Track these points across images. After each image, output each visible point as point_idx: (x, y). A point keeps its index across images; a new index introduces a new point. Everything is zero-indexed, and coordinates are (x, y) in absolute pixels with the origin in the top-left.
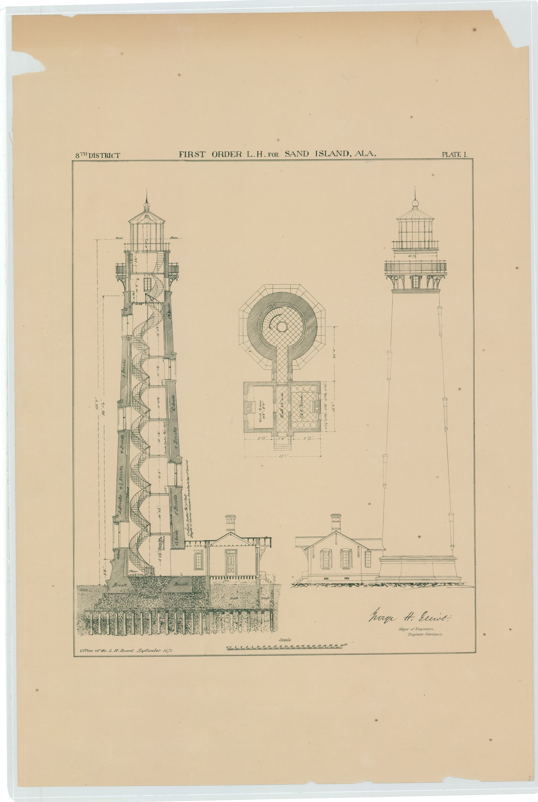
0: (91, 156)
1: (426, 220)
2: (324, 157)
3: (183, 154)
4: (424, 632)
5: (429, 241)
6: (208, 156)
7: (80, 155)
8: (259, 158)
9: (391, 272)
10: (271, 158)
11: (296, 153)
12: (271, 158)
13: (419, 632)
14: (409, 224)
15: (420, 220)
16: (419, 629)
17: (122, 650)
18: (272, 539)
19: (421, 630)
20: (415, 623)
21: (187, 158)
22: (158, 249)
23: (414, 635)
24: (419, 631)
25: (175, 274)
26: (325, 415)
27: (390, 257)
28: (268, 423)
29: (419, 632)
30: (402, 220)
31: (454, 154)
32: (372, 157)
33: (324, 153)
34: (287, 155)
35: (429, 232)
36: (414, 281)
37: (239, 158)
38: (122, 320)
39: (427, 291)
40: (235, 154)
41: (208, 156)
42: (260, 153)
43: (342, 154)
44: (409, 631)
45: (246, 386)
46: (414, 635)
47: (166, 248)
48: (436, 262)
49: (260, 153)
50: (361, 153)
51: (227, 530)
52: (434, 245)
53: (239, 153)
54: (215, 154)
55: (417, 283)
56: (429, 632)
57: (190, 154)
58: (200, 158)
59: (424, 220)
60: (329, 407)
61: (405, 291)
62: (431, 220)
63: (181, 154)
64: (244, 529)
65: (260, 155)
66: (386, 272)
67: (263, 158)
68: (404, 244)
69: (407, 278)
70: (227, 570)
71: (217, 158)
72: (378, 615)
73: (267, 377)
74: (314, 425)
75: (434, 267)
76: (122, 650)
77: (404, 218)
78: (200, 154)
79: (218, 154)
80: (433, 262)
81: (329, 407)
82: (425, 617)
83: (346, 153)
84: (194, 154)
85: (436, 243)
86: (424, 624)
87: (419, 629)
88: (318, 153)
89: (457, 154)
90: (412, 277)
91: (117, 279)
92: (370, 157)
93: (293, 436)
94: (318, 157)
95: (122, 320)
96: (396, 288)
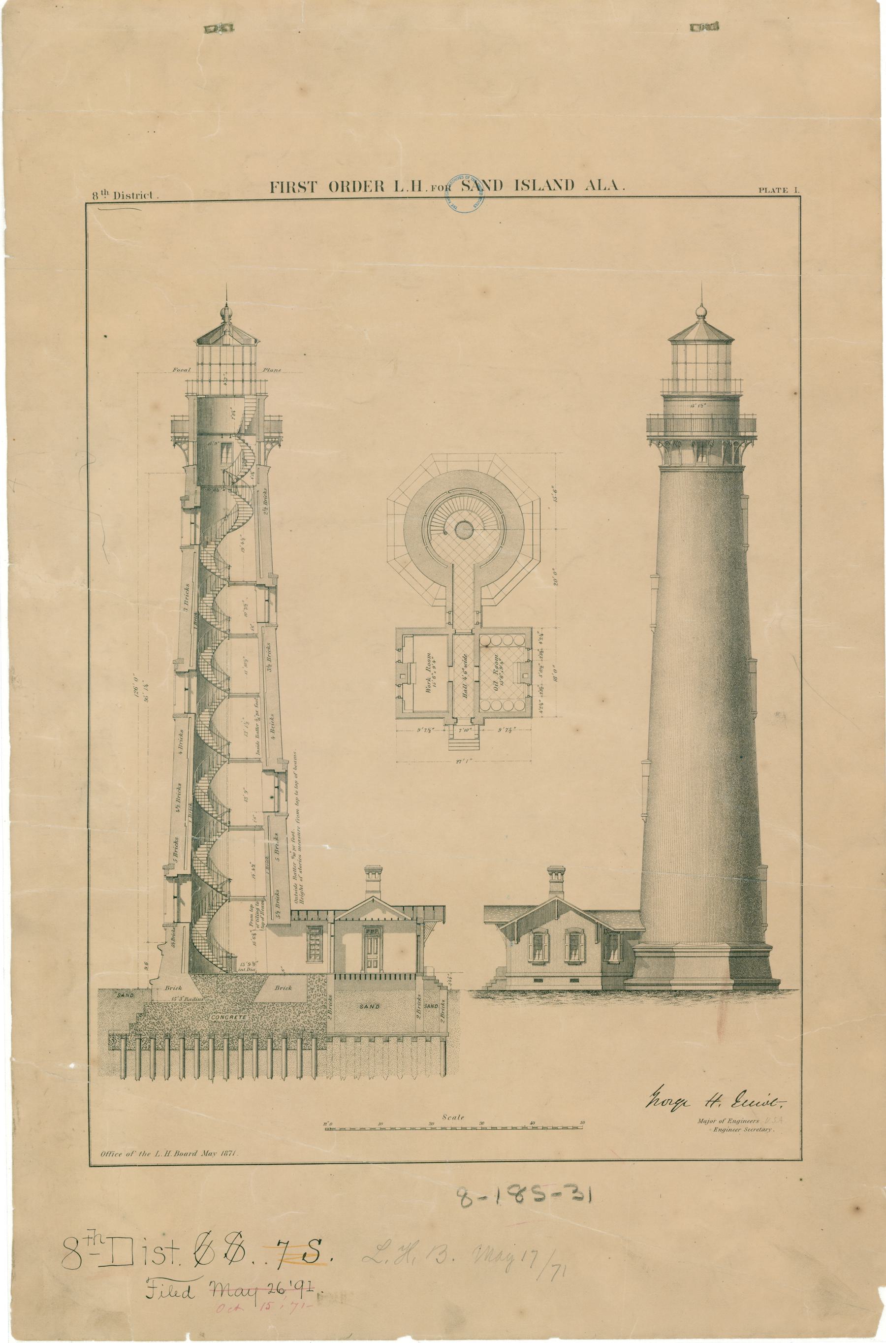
2: (531, 193)
4: (742, 1126)
6: (322, 190)
8: (416, 193)
11: (553, 185)
13: (733, 1126)
16: (734, 1121)
18: (447, 908)
19: (738, 1122)
20: (724, 1110)
22: (247, 391)
25: (277, 435)
26: (541, 689)
28: (437, 701)
29: (733, 1126)
33: (531, 185)
34: (466, 188)
35: (251, 364)
38: (182, 517)
42: (416, 183)
43: (492, 188)
44: (716, 1124)
45: (405, 635)
47: (259, 388)
49: (416, 183)
51: (367, 892)
53: (379, 183)
56: (750, 1126)
60: (548, 672)
64: (398, 890)
65: (416, 188)
66: (648, 434)
68: (682, 384)
70: (366, 964)
73: (438, 619)
74: (520, 706)
76: (177, 1153)
78: (308, 187)
79: (342, 186)
81: (548, 672)
82: (742, 1101)
84: (297, 187)
85: (263, 383)
86: (741, 1113)
87: (734, 1121)
88: (520, 185)
91: (172, 443)
92: (613, 192)
93: (484, 724)
94: (520, 193)
95: (182, 517)
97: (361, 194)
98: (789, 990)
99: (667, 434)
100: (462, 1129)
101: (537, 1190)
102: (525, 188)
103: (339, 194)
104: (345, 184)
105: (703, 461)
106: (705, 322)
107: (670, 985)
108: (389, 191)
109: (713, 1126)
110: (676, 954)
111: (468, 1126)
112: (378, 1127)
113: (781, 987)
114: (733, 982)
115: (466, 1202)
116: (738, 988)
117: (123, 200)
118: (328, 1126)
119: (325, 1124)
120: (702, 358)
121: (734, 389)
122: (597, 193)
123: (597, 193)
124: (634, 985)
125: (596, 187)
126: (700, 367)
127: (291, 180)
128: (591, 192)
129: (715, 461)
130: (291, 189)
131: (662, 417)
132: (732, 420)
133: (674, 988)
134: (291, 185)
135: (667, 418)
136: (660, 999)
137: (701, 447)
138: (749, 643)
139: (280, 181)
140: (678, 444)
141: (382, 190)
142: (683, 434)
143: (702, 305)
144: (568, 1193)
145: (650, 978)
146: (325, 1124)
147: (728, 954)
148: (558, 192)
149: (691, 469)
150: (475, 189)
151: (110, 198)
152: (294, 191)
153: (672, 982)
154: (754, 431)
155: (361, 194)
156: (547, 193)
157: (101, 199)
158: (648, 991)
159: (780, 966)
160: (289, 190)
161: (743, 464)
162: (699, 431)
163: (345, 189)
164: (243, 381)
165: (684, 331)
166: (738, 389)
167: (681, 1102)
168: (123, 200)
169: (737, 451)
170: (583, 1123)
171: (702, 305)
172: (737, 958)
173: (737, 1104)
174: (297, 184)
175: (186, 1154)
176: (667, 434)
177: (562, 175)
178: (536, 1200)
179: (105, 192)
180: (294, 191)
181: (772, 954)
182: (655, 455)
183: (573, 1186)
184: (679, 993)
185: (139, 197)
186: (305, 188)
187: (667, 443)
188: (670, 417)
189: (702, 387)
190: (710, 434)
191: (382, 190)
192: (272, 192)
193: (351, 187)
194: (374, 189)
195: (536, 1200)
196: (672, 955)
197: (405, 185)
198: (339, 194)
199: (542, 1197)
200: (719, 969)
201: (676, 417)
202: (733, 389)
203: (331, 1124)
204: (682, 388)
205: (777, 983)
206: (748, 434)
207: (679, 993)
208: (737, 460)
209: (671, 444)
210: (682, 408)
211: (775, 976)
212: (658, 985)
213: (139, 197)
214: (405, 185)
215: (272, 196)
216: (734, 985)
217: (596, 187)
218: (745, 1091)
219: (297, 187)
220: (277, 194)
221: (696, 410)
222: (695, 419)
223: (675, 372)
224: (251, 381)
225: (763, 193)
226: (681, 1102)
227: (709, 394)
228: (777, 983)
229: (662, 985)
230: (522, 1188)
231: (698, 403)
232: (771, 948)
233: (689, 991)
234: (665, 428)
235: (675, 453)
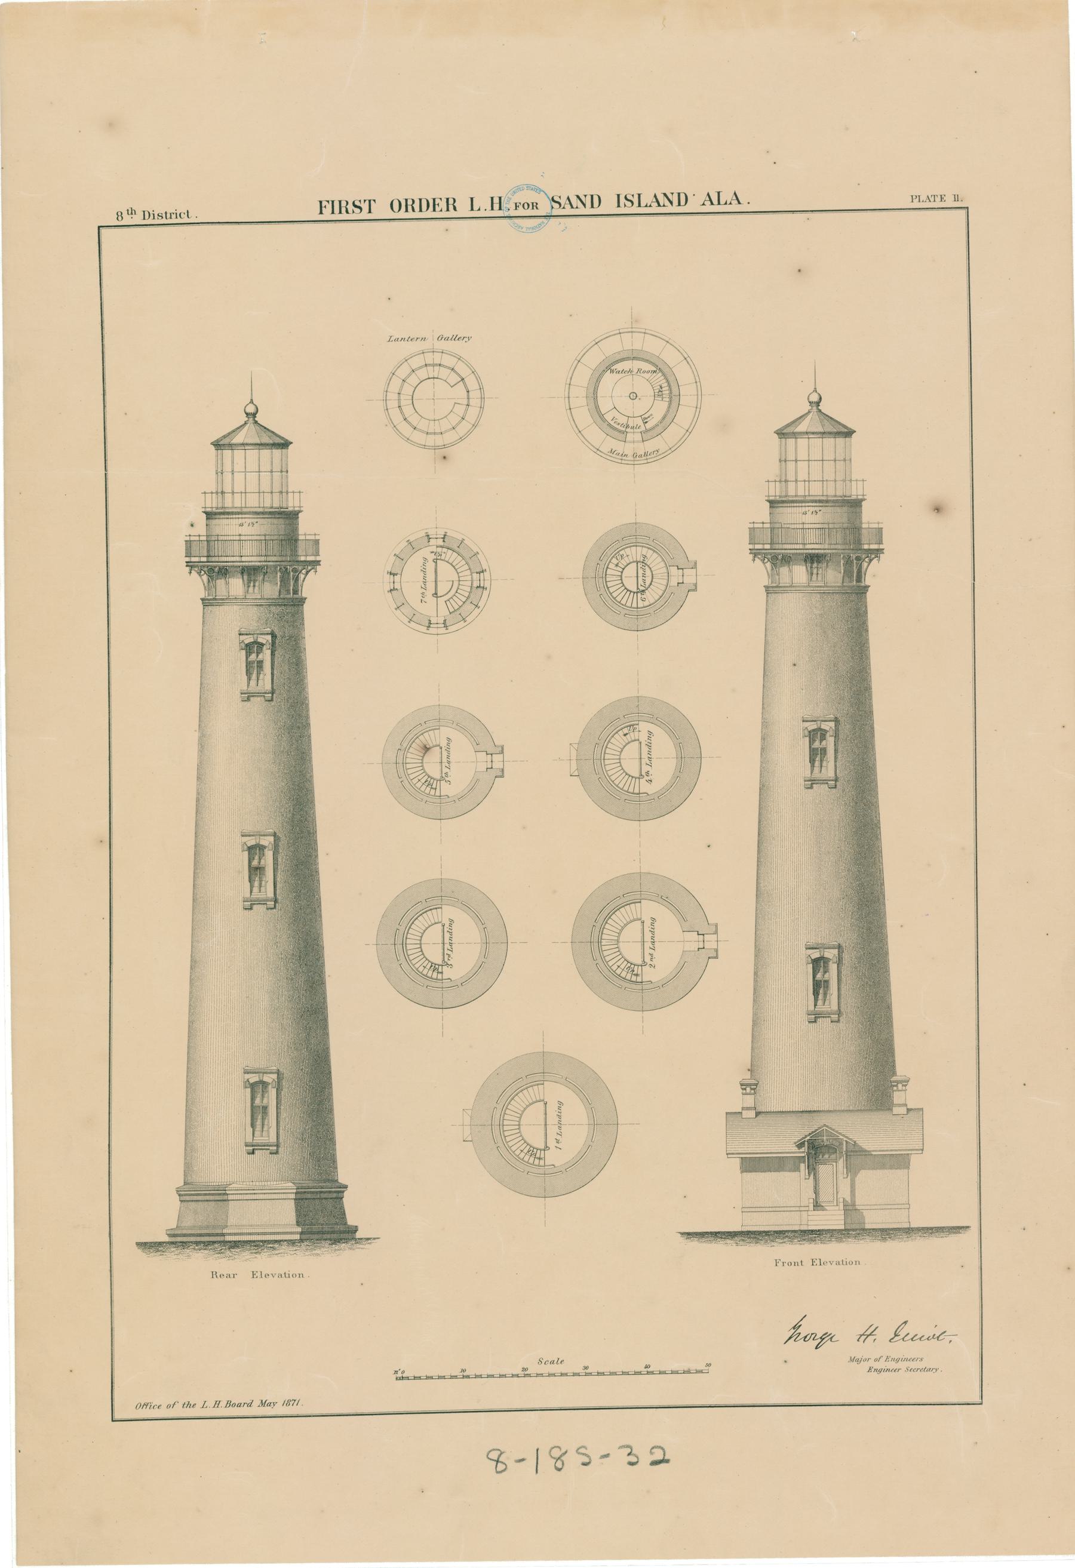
2: (635, 209)
4: (902, 1365)
6: (381, 210)
7: (125, 215)
8: (497, 213)
10: (521, 212)
11: (661, 198)
13: (891, 1365)
16: (893, 1359)
17: (229, 1404)
19: (897, 1361)
21: (337, 217)
23: (879, 1371)
24: (893, 1363)
32: (739, 208)
34: (556, 206)
37: (452, 213)
42: (496, 200)
43: (675, 202)
46: (879, 1371)
49: (496, 200)
50: (496, 203)
53: (451, 201)
56: (913, 1365)
58: (365, 215)
65: (496, 206)
68: (228, 497)
72: (803, 1331)
76: (229, 1404)
78: (365, 207)
79: (406, 205)
82: (902, 1334)
84: (350, 207)
86: (901, 1349)
87: (893, 1359)
92: (735, 207)
97: (430, 214)
98: (368, 1239)
99: (210, 559)
100: (562, 1375)
101: (582, 1450)
102: (629, 204)
103: (402, 214)
104: (410, 202)
105: (255, 593)
106: (256, 422)
107: (223, 1235)
108: (463, 209)
109: (865, 1366)
110: (230, 1197)
111: (570, 1371)
112: (521, 1373)
113: (358, 1235)
114: (299, 1230)
115: (501, 1467)
116: (304, 1237)
117: (154, 220)
118: (399, 1375)
119: (396, 1372)
120: (252, 466)
121: (292, 504)
122: (716, 208)
123: (716, 208)
124: (230, 1234)
125: (715, 201)
126: (250, 478)
127: (343, 198)
128: (708, 208)
129: (270, 589)
130: (343, 210)
131: (204, 538)
132: (291, 539)
133: (228, 1238)
134: (344, 204)
135: (210, 541)
136: (211, 1252)
137: (250, 572)
138: (314, 813)
139: (330, 199)
140: (224, 572)
141: (455, 209)
142: (225, 559)
143: (252, 402)
144: (623, 1456)
145: (201, 1228)
146: (396, 1372)
147: (293, 1196)
148: (582, 210)
149: (242, 601)
150: (568, 206)
151: (138, 219)
152: (347, 212)
153: (225, 1231)
155: (430, 214)
156: (655, 209)
157: (127, 220)
158: (197, 1243)
159: (355, 1210)
160: (339, 211)
161: (304, 595)
162: (250, 556)
163: (410, 208)
165: (229, 434)
166: (297, 504)
167: (827, 1337)
168: (154, 220)
169: (297, 579)
170: (709, 1365)
171: (252, 402)
172: (302, 1199)
173: (897, 1338)
174: (351, 204)
176: (210, 559)
177: (673, 187)
179: (132, 212)
180: (347, 212)
181: (347, 1195)
182: (196, 585)
183: (628, 1446)
184: (235, 1245)
185: (174, 216)
186: (360, 208)
187: (211, 570)
188: (213, 538)
189: (253, 502)
190: (263, 559)
191: (455, 209)
192: (321, 213)
193: (416, 206)
194: (445, 208)
195: (584, 1464)
196: (225, 1197)
197: (482, 202)
198: (402, 214)
199: (587, 1460)
200: (282, 1215)
201: (221, 538)
202: (290, 504)
203: (403, 1372)
204: (228, 503)
205: (355, 1230)
206: (309, 558)
207: (235, 1245)
208: (295, 592)
209: (215, 572)
210: (228, 527)
211: (351, 1221)
212: (209, 1235)
213: (174, 216)
214: (482, 202)
215: (321, 217)
216: (302, 1233)
217: (715, 201)
218: (905, 1322)
219: (350, 207)
220: (327, 214)
221: (246, 530)
222: (244, 539)
223: (220, 481)
225: (916, 205)
226: (827, 1337)
227: (261, 510)
228: (355, 1230)
229: (278, 1233)
230: (563, 1451)
231: (249, 521)
232: (346, 1187)
233: (247, 1242)
234: (208, 551)
235: (220, 583)
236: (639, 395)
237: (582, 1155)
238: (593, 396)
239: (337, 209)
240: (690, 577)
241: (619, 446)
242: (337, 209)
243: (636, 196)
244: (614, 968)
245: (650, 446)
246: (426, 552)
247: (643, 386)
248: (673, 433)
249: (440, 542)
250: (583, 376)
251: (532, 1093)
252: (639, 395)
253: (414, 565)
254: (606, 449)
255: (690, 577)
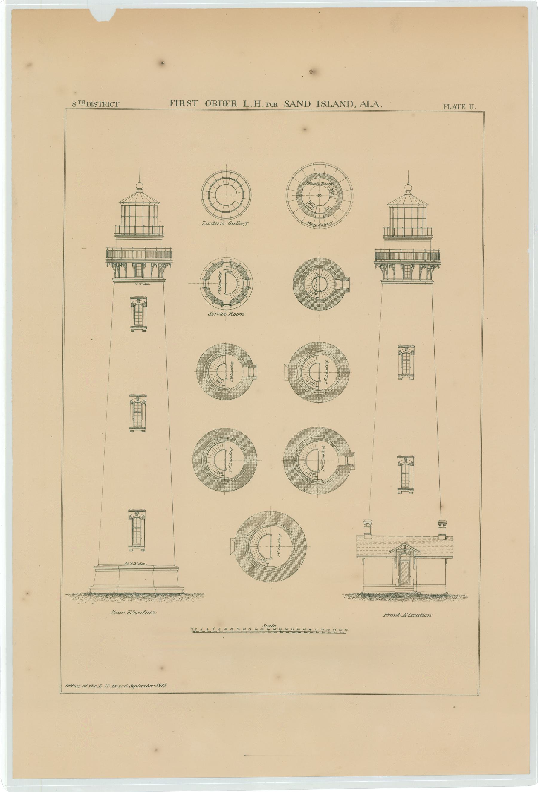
0: (89, 105)
1: (151, 204)
3: (175, 103)
5: (422, 228)
6: (201, 105)
8: (257, 108)
9: (115, 260)
11: (296, 103)
12: (269, 108)
14: (133, 208)
15: (413, 206)
27: (112, 243)
30: (125, 204)
31: (457, 107)
33: (327, 103)
34: (287, 105)
35: (154, 217)
36: (138, 268)
38: (421, 272)
39: (420, 282)
40: (230, 104)
41: (201, 105)
42: (257, 102)
43: (346, 105)
48: (429, 252)
49: (257, 102)
50: (366, 104)
52: (156, 231)
53: (182, 102)
54: (208, 104)
55: (409, 273)
57: (182, 103)
59: (148, 204)
61: (394, 282)
62: (425, 206)
63: (267, 105)
65: (257, 105)
67: (261, 108)
69: (130, 265)
71: (211, 107)
75: (428, 257)
76: (114, 686)
77: (396, 203)
78: (193, 103)
79: (212, 103)
80: (426, 252)
83: (350, 104)
84: (186, 103)
85: (161, 228)
89: (461, 107)
90: (134, 265)
95: (421, 272)
96: (386, 277)
143: (408, 184)
154: (439, 260)
164: (418, 218)
171: (408, 184)
175: (119, 686)
178: (164, 685)
215: (171, 107)
224: (149, 217)
236: (321, 194)
237: (240, 474)
238: (299, 195)
239: (178, 104)
240: (346, 285)
241: (312, 220)
242: (178, 104)
243: (304, 102)
244: (304, 473)
245: (328, 220)
246: (221, 269)
247: (324, 191)
248: (339, 214)
249: (228, 265)
250: (295, 186)
251: (219, 446)
252: (321, 194)
253: (215, 275)
254: (305, 221)
255: (346, 285)
